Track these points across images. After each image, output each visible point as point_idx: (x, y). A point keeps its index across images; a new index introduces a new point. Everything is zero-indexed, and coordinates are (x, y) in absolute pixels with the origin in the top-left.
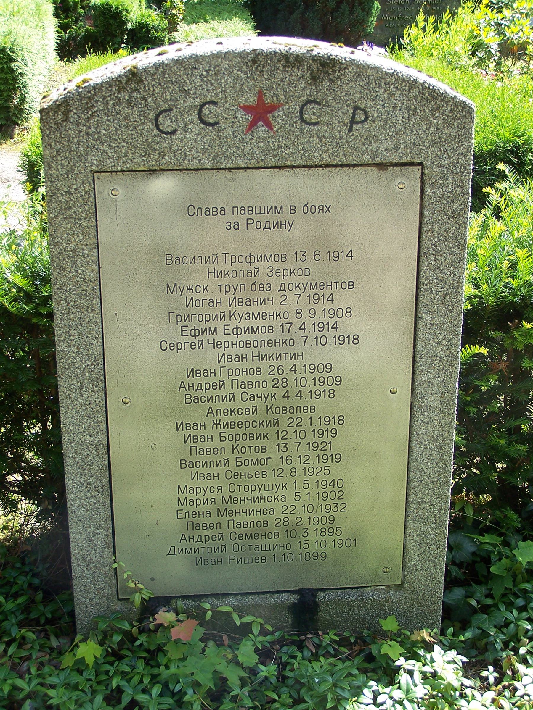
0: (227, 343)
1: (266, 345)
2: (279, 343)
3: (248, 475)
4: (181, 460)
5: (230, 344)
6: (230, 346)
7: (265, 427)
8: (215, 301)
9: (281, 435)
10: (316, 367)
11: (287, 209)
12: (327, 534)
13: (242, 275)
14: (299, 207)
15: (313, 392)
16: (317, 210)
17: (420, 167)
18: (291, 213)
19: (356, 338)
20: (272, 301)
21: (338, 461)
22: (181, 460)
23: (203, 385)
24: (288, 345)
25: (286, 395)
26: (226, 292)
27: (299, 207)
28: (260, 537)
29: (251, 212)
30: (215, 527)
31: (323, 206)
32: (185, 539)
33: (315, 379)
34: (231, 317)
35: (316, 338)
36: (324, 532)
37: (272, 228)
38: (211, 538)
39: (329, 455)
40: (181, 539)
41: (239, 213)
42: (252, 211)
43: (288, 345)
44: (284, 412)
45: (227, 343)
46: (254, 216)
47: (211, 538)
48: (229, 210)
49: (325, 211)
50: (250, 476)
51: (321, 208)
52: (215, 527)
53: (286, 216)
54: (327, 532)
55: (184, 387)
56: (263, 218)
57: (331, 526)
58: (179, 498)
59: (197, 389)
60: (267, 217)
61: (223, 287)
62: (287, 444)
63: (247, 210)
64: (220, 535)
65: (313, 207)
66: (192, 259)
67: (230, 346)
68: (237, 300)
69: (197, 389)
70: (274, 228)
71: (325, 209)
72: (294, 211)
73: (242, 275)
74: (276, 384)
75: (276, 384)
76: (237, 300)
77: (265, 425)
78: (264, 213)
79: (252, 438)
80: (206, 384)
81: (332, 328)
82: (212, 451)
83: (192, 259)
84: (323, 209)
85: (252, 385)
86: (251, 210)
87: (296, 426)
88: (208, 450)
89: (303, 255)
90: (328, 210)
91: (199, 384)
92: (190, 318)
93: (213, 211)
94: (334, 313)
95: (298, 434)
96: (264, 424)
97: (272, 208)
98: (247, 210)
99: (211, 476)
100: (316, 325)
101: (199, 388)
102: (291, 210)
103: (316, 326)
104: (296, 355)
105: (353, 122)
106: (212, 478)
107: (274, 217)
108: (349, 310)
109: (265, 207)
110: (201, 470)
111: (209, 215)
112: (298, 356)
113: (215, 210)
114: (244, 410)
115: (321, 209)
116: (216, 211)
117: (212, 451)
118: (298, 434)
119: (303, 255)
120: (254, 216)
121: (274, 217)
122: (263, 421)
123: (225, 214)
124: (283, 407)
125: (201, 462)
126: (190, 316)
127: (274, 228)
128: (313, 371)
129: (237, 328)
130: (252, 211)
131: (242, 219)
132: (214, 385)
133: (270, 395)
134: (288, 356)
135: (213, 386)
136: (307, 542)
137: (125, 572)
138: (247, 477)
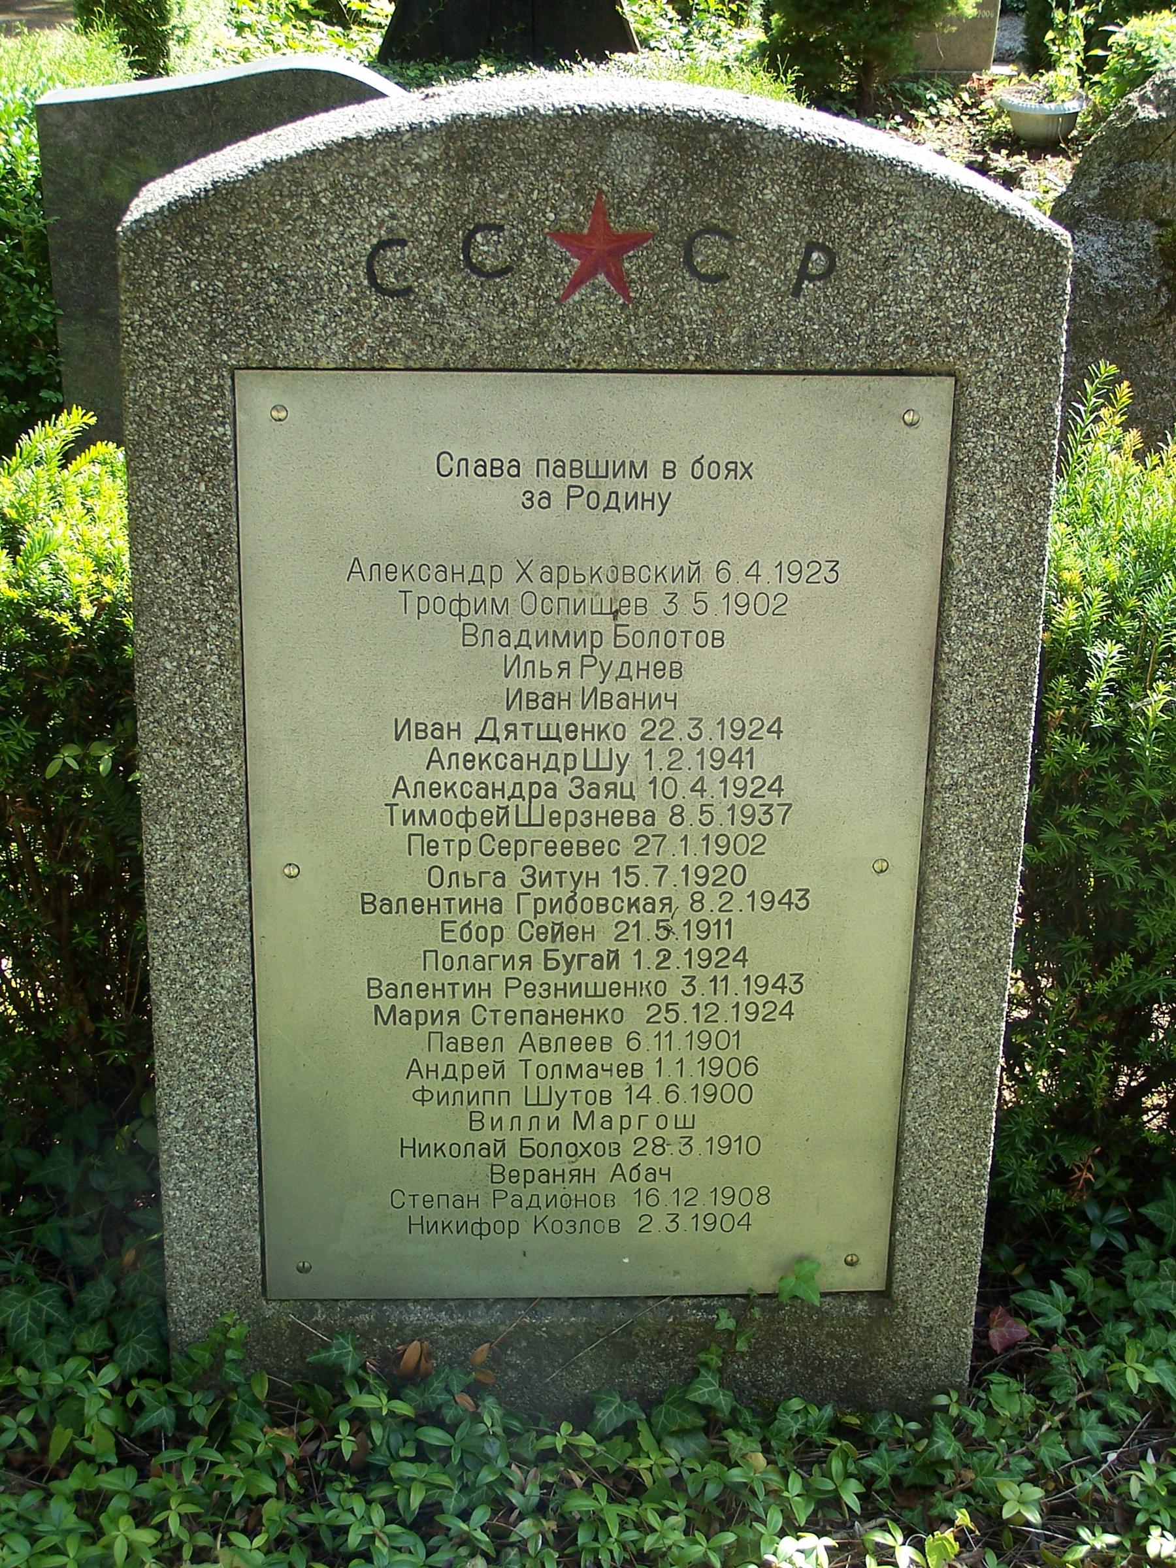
4: (369, 980)
8: (631, 696)
9: (684, 1198)
10: (719, 1092)
11: (655, 468)
14: (684, 470)
15: (691, 870)
18: (665, 477)
20: (674, 701)
21: (753, 1017)
22: (369, 980)
24: (611, 737)
27: (684, 470)
28: (580, 934)
29: (499, 472)
30: (490, 1046)
33: (701, 752)
35: (654, 781)
37: (534, 646)
38: (476, 1071)
39: (713, 921)
42: (580, 469)
43: (611, 737)
44: (602, 909)
46: (583, 481)
47: (476, 1071)
48: (528, 471)
51: (731, 466)
52: (490, 1046)
53: (652, 483)
57: (712, 1080)
64: (498, 1066)
65: (714, 465)
70: (627, 508)
71: (741, 471)
77: (454, 1230)
78: (606, 476)
82: (475, 1045)
84: (735, 470)
86: (578, 467)
87: (661, 739)
90: (747, 470)
92: (472, 609)
93: (492, 468)
96: (453, 1226)
97: (623, 464)
101: (517, 793)
103: (785, 569)
104: (473, 902)
105: (803, 274)
106: (551, 1179)
107: (625, 485)
111: (485, 475)
112: (477, 905)
115: (732, 468)
116: (501, 468)
117: (475, 1045)
121: (625, 485)
124: (598, 899)
127: (627, 508)
130: (580, 469)
131: (558, 488)
136: (675, 1007)
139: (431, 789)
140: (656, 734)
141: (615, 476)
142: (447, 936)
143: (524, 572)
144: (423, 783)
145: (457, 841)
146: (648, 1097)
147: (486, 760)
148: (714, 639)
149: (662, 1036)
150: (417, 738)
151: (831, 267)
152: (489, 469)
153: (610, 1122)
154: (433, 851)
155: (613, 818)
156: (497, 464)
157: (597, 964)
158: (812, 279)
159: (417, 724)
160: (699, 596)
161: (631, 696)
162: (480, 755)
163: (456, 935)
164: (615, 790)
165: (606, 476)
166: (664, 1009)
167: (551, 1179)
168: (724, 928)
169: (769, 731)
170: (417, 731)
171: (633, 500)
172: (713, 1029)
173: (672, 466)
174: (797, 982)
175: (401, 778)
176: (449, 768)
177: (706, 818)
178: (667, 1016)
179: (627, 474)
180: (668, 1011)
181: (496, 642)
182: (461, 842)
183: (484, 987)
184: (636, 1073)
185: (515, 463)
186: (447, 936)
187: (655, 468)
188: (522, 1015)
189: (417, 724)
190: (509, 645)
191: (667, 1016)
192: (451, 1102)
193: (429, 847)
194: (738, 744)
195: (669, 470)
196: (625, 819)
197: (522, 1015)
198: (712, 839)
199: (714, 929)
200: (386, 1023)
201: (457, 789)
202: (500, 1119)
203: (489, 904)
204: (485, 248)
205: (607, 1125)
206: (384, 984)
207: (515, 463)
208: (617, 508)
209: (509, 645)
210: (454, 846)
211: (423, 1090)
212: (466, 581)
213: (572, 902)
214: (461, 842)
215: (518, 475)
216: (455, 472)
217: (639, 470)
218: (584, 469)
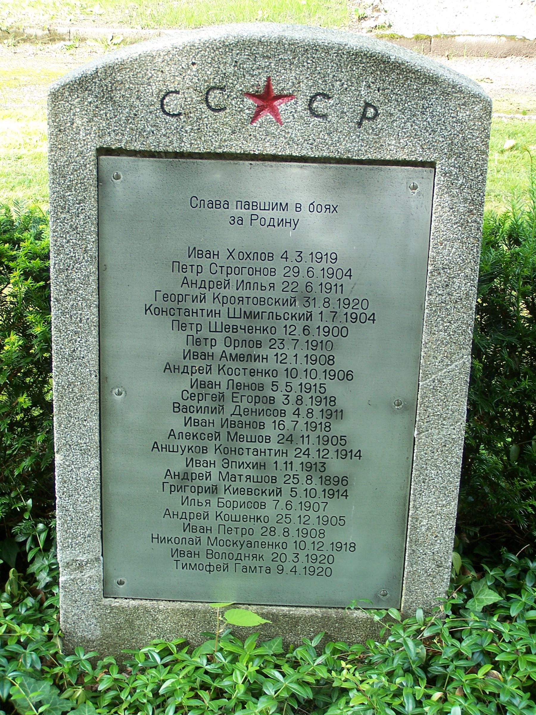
1: (206, 206)
2: (260, 330)
13: (202, 205)
16: (324, 209)
19: (353, 546)
21: (314, 429)
23: (188, 515)
25: (297, 413)
26: (228, 274)
31: (330, 205)
32: (169, 514)
40: (165, 514)
46: (258, 212)
48: (233, 205)
49: (331, 211)
54: (331, 480)
55: (187, 283)
56: (268, 215)
61: (224, 269)
62: (288, 396)
66: (243, 506)
68: (229, 422)
71: (332, 209)
72: (299, 209)
73: (202, 205)
76: (229, 422)
78: (269, 210)
79: (250, 493)
81: (355, 456)
83: (243, 506)
84: (329, 209)
86: (255, 205)
90: (335, 209)
91: (202, 281)
94: (307, 533)
97: (277, 204)
99: (206, 423)
100: (323, 285)
102: (296, 207)
105: (364, 116)
106: (193, 556)
107: (277, 214)
109: (262, 319)
110: (195, 416)
113: (218, 203)
120: (258, 212)
121: (277, 214)
125: (195, 407)
128: (309, 469)
131: (245, 213)
132: (198, 516)
133: (187, 448)
134: (205, 312)
135: (199, 476)
137: (117, 387)
139: (186, 436)
140: (289, 288)
141: (273, 209)
142: (235, 400)
143: (231, 255)
145: (210, 339)
146: (350, 276)
151: (376, 115)
152: (214, 204)
153: (270, 570)
155: (249, 330)
156: (218, 203)
157: (244, 570)
158: (369, 119)
160: (341, 518)
162: (193, 433)
163: (239, 400)
164: (250, 479)
166: (292, 477)
167: (193, 556)
168: (339, 288)
169: (304, 454)
172: (319, 553)
173: (272, 255)
174: (322, 466)
176: (179, 439)
177: (294, 494)
179: (279, 209)
180: (294, 478)
182: (212, 339)
183: (216, 253)
185: (208, 252)
186: (235, 400)
187: (292, 207)
192: (203, 412)
193: (196, 342)
194: (346, 310)
195: (298, 207)
198: (349, 315)
200: (224, 480)
204: (215, 98)
205: (268, 571)
206: (181, 405)
207: (208, 252)
208: (274, 226)
212: (180, 372)
213: (311, 205)
214: (212, 339)
215: (228, 208)
216: (199, 205)
217: (284, 207)
218: (258, 206)
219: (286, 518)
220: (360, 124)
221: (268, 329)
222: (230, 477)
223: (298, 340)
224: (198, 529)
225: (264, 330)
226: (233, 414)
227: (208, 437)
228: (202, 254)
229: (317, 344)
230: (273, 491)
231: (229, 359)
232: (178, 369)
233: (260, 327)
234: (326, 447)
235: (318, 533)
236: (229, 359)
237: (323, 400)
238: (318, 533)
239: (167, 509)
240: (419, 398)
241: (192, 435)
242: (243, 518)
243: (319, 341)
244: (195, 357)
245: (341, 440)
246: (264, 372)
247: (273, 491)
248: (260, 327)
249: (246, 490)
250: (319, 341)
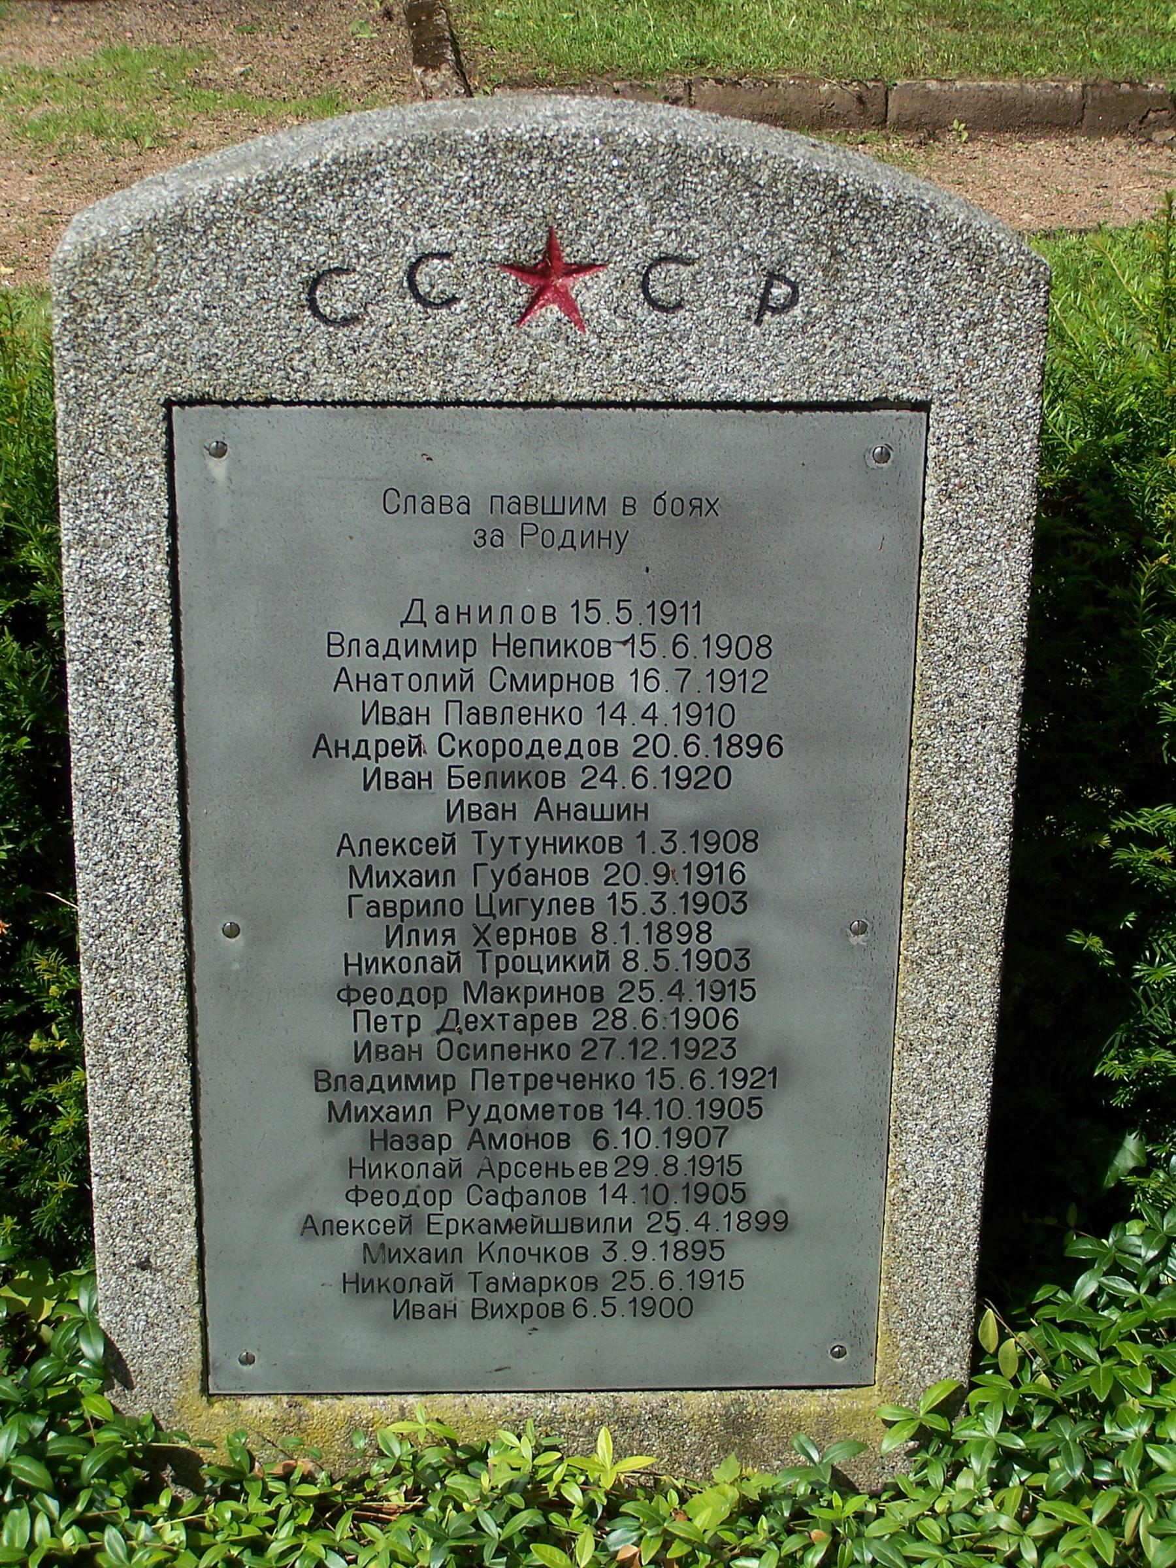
0: (520, 932)
3: (564, 1169)
5: (528, 934)
6: (528, 939)
7: (578, 969)
8: (500, 807)
10: (711, 1193)
12: (674, 939)
13: (354, 651)
17: (175, 409)
32: (348, 682)
34: (481, 1255)
36: (747, 1221)
40: (338, 682)
41: (505, 508)
45: (520, 932)
48: (479, 508)
50: (568, 1173)
53: (611, 520)
54: (673, 931)
58: (352, 869)
59: (357, 755)
60: (568, 521)
63: (523, 504)
64: (448, 839)
66: (564, 842)
67: (528, 939)
69: (357, 755)
71: (706, 506)
73: (354, 651)
74: (650, 1051)
75: (650, 1051)
80: (377, 742)
84: (700, 507)
85: (494, 715)
88: (607, 652)
89: (738, 901)
90: (712, 506)
94: (730, 647)
95: (716, 713)
96: (576, 962)
97: (416, 642)
98: (523, 504)
102: (625, 505)
108: (764, 641)
111: (478, 722)
114: (424, 842)
118: (716, 713)
119: (738, 901)
122: (573, 957)
123: (468, 512)
126: (567, 510)
129: (512, 1193)
131: (511, 524)
138: (560, 1173)
139: (378, 847)
144: (369, 841)
147: (572, 646)
148: (602, 682)
149: (690, 607)
150: (387, 787)
154: (380, 1027)
158: (774, 311)
159: (387, 773)
161: (500, 807)
162: (394, 841)
165: (563, 513)
166: (638, 985)
170: (387, 780)
171: (593, 539)
174: (743, 958)
175: (345, 835)
176: (361, 855)
178: (743, 992)
180: (642, 989)
181: (429, 968)
182: (410, 1017)
184: (580, 1258)
188: (493, 1050)
189: (387, 773)
190: (377, 655)
191: (743, 992)
195: (629, 506)
196: (562, 1023)
197: (493, 1050)
199: (680, 612)
201: (406, 845)
202: (490, 608)
203: (573, 809)
209: (377, 655)
210: (403, 1022)
211: (356, 1190)
214: (410, 1017)
217: (596, 505)
218: (539, 505)
219: (633, 1278)
220: (760, 313)
221: (565, 714)
222: (489, 992)
223: (614, 1040)
224: (426, 1311)
225: (608, 1083)
226: (406, 621)
227: (428, 846)
228: (392, 716)
229: (698, 1044)
230: (590, 958)
231: (487, 1146)
232: (346, 748)
233: (555, 839)
234: (703, 917)
235: (742, 841)
236: (487, 1146)
237: (678, 609)
238: (742, 841)
239: (343, 669)
240: (904, 931)
241: (391, 844)
242: (520, 716)
243: (717, 1272)
244: (391, 784)
245: (750, 1106)
246: (556, 997)
247: (590, 958)
248: (555, 839)
249: (562, 1020)
250: (717, 1272)
